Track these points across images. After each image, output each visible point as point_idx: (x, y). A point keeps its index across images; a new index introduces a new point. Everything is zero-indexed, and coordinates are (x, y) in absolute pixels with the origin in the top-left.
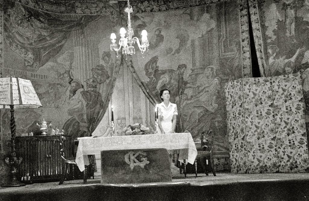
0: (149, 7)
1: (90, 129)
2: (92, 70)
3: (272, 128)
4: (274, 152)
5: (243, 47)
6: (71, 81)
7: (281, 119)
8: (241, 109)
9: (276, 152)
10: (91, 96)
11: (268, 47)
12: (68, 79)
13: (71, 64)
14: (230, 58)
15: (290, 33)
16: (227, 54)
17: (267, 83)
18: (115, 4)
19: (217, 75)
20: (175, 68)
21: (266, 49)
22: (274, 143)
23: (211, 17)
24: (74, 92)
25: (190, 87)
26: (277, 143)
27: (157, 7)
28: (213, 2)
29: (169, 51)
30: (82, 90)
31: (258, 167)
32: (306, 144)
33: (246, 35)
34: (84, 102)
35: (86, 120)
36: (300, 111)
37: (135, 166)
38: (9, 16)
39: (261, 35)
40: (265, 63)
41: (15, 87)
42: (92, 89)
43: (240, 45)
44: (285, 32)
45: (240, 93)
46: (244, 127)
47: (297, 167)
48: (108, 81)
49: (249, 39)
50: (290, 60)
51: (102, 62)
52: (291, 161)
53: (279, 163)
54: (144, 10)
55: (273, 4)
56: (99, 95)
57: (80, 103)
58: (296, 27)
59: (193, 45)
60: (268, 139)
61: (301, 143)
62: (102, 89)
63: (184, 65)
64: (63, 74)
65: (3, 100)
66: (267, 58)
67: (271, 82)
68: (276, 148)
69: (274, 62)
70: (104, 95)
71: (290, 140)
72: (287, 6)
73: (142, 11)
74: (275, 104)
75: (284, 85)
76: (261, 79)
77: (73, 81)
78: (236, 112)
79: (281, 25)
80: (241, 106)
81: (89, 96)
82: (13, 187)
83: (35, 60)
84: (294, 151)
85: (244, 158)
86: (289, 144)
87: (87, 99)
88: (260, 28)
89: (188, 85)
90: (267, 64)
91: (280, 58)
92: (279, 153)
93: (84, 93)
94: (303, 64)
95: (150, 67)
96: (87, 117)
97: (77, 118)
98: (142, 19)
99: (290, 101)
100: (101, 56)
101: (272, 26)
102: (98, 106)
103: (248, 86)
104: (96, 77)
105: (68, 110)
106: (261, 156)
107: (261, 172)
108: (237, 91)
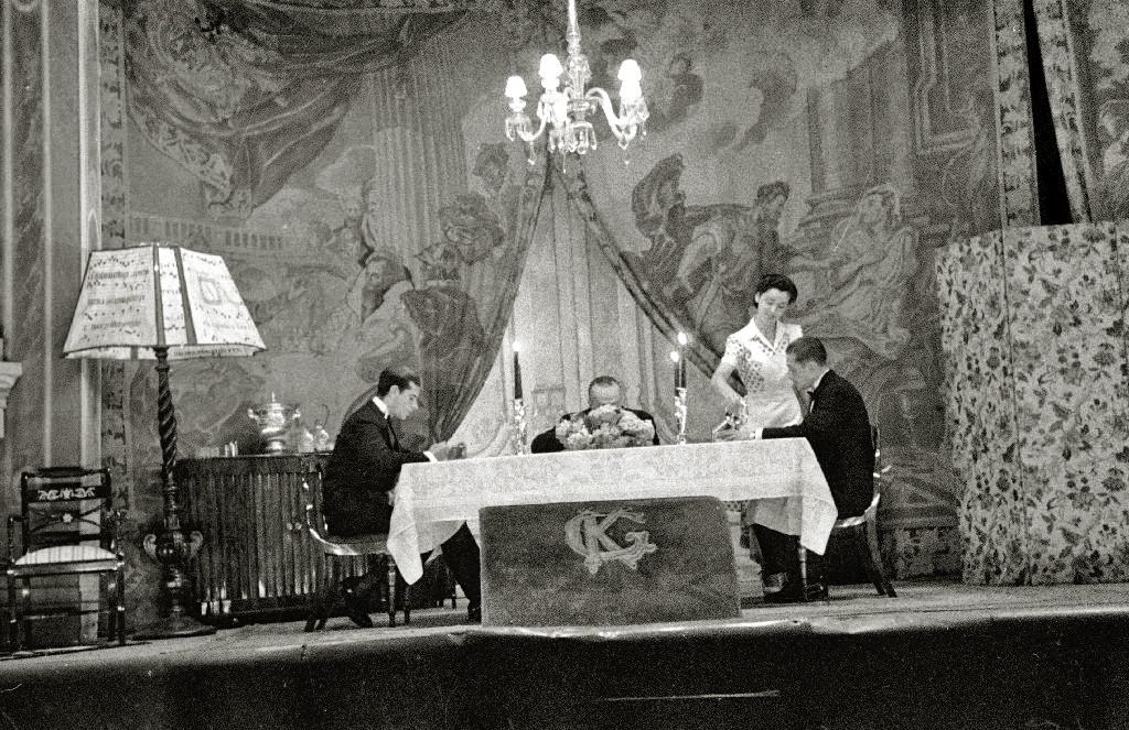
5: (1004, 111)
12: (354, 248)
13: (364, 194)
14: (953, 153)
19: (906, 219)
20: (746, 198)
24: (378, 296)
25: (804, 268)
29: (722, 136)
30: (402, 287)
31: (1068, 560)
33: (1016, 64)
34: (414, 329)
38: (142, 23)
40: (1087, 167)
41: (170, 283)
42: (443, 284)
45: (996, 286)
48: (498, 253)
49: (1025, 82)
51: (476, 185)
56: (466, 305)
57: (401, 334)
59: (812, 107)
62: (479, 283)
63: (779, 184)
65: (128, 328)
66: (1096, 157)
67: (1113, 244)
76: (1076, 232)
77: (374, 255)
93: (415, 300)
98: (619, 19)
102: (465, 344)
103: (1023, 259)
104: (456, 239)
107: (1078, 580)
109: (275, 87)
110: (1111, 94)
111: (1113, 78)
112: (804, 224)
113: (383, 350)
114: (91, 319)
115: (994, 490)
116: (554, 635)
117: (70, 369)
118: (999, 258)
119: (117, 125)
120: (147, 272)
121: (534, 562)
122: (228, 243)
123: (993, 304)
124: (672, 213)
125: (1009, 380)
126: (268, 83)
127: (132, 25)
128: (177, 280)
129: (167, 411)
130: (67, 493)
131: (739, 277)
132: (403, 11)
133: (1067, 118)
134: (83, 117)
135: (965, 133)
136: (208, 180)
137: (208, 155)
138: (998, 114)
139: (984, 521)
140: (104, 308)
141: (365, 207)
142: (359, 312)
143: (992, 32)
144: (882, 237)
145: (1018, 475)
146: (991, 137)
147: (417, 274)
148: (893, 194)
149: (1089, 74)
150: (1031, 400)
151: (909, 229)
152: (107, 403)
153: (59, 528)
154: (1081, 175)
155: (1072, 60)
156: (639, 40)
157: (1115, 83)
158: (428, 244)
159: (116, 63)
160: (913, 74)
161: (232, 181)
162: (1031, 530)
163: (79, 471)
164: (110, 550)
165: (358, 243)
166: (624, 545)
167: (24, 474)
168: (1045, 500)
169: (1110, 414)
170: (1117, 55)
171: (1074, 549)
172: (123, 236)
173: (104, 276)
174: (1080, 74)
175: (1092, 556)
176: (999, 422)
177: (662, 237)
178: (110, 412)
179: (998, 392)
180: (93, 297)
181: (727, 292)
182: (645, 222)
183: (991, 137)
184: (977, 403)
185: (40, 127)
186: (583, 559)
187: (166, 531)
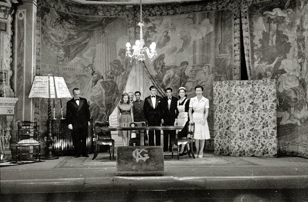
0: (159, 11)
1: (108, 113)
2: (110, 64)
3: (251, 121)
4: (251, 140)
5: (235, 51)
6: (93, 73)
7: (259, 114)
8: (227, 105)
9: (253, 141)
10: (109, 85)
11: (255, 53)
12: (91, 71)
13: (94, 58)
14: (223, 58)
15: (272, 43)
16: (222, 55)
17: (249, 85)
18: (131, 8)
19: (213, 72)
20: (178, 64)
21: (253, 55)
22: (252, 133)
23: (211, 23)
24: (95, 82)
25: (190, 81)
26: (254, 133)
27: (166, 11)
28: (213, 9)
29: (174, 50)
30: (101, 80)
31: (238, 151)
32: (276, 135)
33: (237, 41)
34: (103, 90)
35: (104, 106)
36: (273, 110)
37: (139, 160)
38: (45, 20)
39: (250, 42)
40: (251, 65)
41: (52, 84)
42: (110, 80)
43: (232, 49)
44: (268, 42)
45: (227, 92)
46: (229, 119)
47: (268, 153)
48: (123, 73)
49: (239, 45)
50: (270, 65)
51: (119, 58)
52: (264, 148)
53: (255, 149)
54: (154, 14)
55: (261, 17)
56: (115, 85)
57: (100, 91)
58: (276, 38)
59: (194, 46)
60: (248, 130)
61: (272, 134)
62: (118, 81)
63: (186, 62)
64: (87, 67)
65: (43, 94)
66: (253, 63)
67: (253, 85)
68: (253, 137)
69: (258, 67)
70: (119, 85)
71: (264, 132)
72: (271, 20)
73: (153, 15)
74: (255, 102)
75: (262, 88)
76: (245, 82)
77: (95, 73)
78: (222, 107)
79: (266, 35)
80: (227, 103)
81: (107, 86)
82: (50, 159)
83: (65, 56)
84: (266, 141)
85: (228, 144)
86: (263, 135)
87: (105, 87)
88: (249, 36)
89: (189, 80)
90: (253, 67)
91: (263, 63)
92: (255, 141)
93: (103, 83)
94: (280, 70)
95: (158, 63)
96: (106, 102)
97: (98, 104)
98: (153, 22)
99: (266, 101)
100: (118, 52)
101: (258, 35)
102: (115, 94)
103: (234, 87)
104: (113, 70)
105: (91, 97)
106: (241, 143)
107: (240, 156)
108: (225, 91)
109: (74, 34)
110: (257, 50)
111: (258, 47)
112: (191, 71)
113: (96, 95)
114: (34, 91)
115: (224, 135)
116: (129, 179)
117: (28, 100)
118: (229, 87)
119: (39, 44)
120: (47, 82)
121: (127, 159)
122: (63, 70)
123: (227, 96)
124: (162, 67)
125: (229, 113)
126: (73, 33)
127: (43, 21)
128: (54, 83)
129: (50, 111)
130: (28, 127)
131: (176, 82)
132: (104, 17)
133: (247, 54)
134: (33, 44)
135: (227, 54)
136: (59, 55)
137: (59, 50)
138: (233, 51)
139: (221, 142)
140: (37, 89)
141: (93, 62)
142: (91, 85)
143: (233, 33)
144: (207, 75)
145: (230, 133)
146: (231, 56)
147: (104, 77)
148: (210, 66)
149: (253, 45)
150: (233, 117)
151: (213, 74)
152: (36, 107)
153: (26, 134)
154: (249, 67)
155: (249, 41)
156: (157, 27)
157: (258, 48)
158: (107, 71)
159: (39, 30)
160: (216, 40)
161: (64, 55)
162: (231, 145)
163: (29, 122)
164: (37, 140)
165: (91, 70)
166: (144, 157)
167: (19, 123)
168: (235, 138)
169: (272, 92)
170: (259, 42)
171: (263, 121)
172: (39, 69)
173: (38, 82)
174: (251, 44)
175: (243, 151)
176: (226, 121)
177: (159, 72)
178: (36, 108)
179: (226, 115)
180: (35, 86)
181: (173, 85)
182: (156, 68)
183: (231, 56)
184: (221, 116)
185: (23, 46)
186: (135, 159)
187: (49, 136)
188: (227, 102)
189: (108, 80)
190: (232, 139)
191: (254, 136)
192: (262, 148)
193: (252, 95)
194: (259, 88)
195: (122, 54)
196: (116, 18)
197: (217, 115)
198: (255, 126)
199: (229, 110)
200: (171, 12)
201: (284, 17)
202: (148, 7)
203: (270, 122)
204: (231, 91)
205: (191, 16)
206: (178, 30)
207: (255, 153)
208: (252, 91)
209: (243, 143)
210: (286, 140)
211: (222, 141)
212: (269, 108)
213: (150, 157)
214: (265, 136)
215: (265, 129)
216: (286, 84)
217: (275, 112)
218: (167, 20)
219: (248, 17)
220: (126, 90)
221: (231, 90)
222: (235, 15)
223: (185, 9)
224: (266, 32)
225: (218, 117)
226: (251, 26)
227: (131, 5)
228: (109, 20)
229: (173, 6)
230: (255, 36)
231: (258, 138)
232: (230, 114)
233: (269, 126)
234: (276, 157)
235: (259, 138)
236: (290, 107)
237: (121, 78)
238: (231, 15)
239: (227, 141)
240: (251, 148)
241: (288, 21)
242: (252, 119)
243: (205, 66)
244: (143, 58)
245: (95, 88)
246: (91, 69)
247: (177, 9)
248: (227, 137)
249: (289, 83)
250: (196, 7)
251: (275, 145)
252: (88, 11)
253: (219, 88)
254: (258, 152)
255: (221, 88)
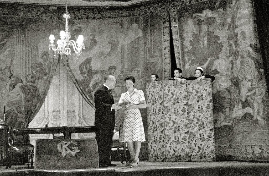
0: (85, 14)
2: (31, 67)
3: (187, 152)
4: (187, 144)
5: (165, 54)
7: (194, 116)
8: (161, 134)
9: (189, 144)
13: (12, 61)
14: (153, 63)
15: (203, 44)
17: (183, 85)
18: (55, 10)
21: (183, 57)
22: (188, 136)
23: (139, 27)
24: (13, 86)
26: (190, 136)
29: (102, 54)
30: (21, 84)
31: (174, 156)
32: (213, 137)
33: (167, 44)
34: (23, 95)
36: (211, 139)
45: (161, 93)
47: (205, 157)
48: (45, 77)
49: (169, 48)
51: (41, 61)
52: (201, 151)
53: (191, 153)
56: (37, 89)
62: (40, 85)
63: (114, 66)
67: (187, 85)
68: (189, 140)
70: (41, 90)
71: (200, 134)
72: (201, 22)
73: (79, 18)
75: (197, 88)
77: (13, 76)
78: (156, 136)
79: (196, 37)
80: (161, 104)
93: (23, 88)
96: (25, 108)
97: (15, 111)
98: (78, 25)
101: (189, 37)
102: (35, 100)
103: (167, 87)
107: (176, 161)
113: (14, 100)
118: (162, 87)
123: (160, 97)
124: (89, 71)
125: (163, 115)
138: (163, 55)
141: (11, 64)
145: (164, 136)
147: (24, 82)
149: (183, 47)
157: (188, 50)
160: (145, 44)
165: (9, 73)
166: (72, 150)
177: (86, 76)
182: (82, 73)
183: (162, 59)
188: (160, 104)
189: (28, 84)
190: (167, 143)
191: (190, 139)
192: (199, 152)
193: (187, 124)
194: (193, 88)
195: (45, 56)
196: (38, 19)
197: (150, 118)
198: (191, 128)
199: (162, 112)
200: (98, 16)
201: (215, 18)
202: (73, 10)
203: (205, 94)
204: (164, 92)
205: (119, 21)
206: (106, 35)
207: (192, 157)
208: (186, 91)
209: (178, 118)
210: (222, 144)
211: (156, 146)
212: (204, 108)
213: (80, 150)
214: (202, 138)
215: (201, 131)
216: (220, 85)
217: (212, 142)
218: (93, 24)
219: (177, 20)
220: (49, 96)
221: (164, 91)
222: (164, 19)
223: (114, 14)
224: (196, 33)
225: (152, 121)
226: (181, 29)
227: (54, 6)
228: (31, 21)
229: (100, 10)
230: (185, 38)
231: (194, 141)
232: (164, 116)
233: (206, 127)
234: (214, 161)
235: (196, 141)
236: (225, 108)
237: (43, 82)
238: (160, 20)
239: (161, 146)
240: (187, 152)
241: (219, 21)
242: (186, 122)
243: (134, 70)
244: (69, 52)
245: (13, 92)
246: (8, 71)
247: (104, 14)
248: (162, 141)
249: (222, 84)
250: (124, 13)
251: (213, 148)
252: (6, 11)
253: (152, 90)
254: (193, 127)
255: (155, 87)
